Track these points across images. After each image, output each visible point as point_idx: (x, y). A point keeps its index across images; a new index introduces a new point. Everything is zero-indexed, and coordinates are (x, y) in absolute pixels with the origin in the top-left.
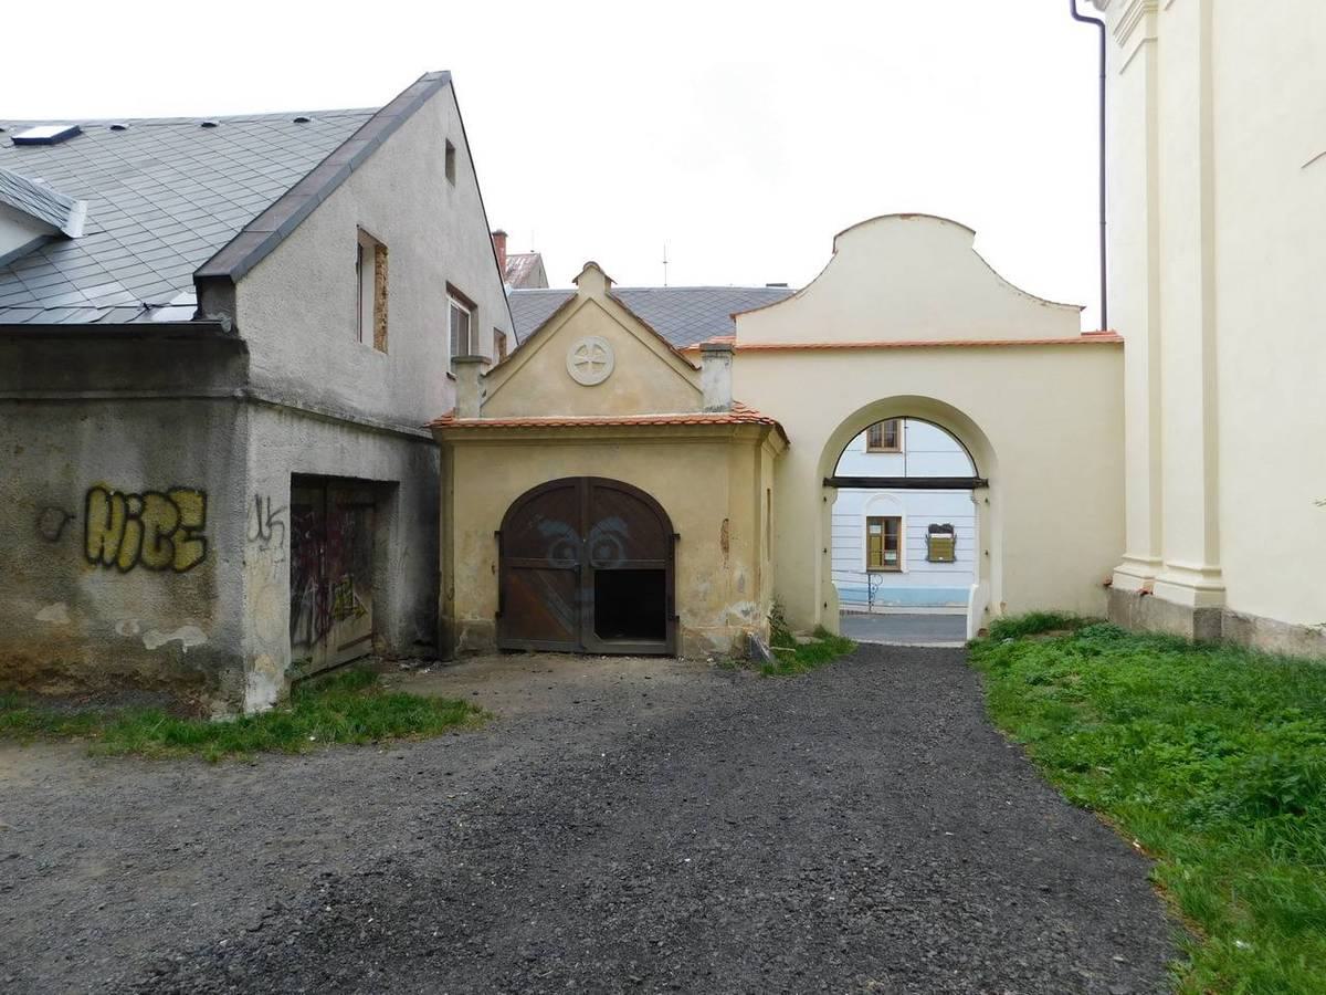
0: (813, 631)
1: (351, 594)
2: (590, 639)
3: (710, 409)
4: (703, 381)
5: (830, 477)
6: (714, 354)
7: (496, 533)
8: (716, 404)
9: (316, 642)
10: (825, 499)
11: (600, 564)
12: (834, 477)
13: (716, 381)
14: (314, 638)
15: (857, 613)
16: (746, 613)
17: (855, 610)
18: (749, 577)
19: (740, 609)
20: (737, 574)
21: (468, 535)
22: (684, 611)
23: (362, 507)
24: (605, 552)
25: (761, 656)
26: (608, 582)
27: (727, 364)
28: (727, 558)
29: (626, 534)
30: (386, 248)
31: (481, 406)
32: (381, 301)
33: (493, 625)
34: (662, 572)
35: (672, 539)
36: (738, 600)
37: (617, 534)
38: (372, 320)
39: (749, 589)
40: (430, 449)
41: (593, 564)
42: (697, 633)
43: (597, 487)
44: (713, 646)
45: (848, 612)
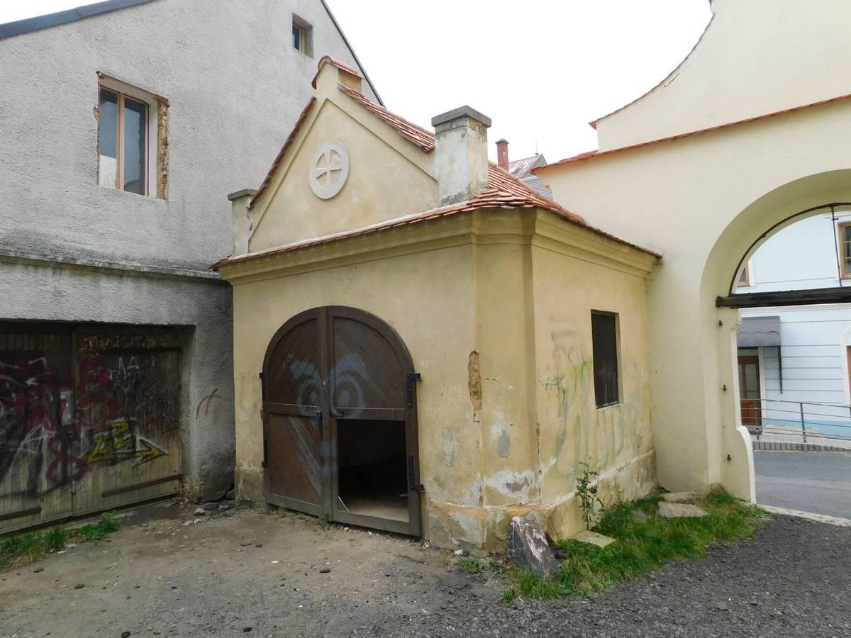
0: (705, 491)
1: (133, 438)
2: (333, 505)
3: (446, 201)
4: (437, 165)
5: (725, 294)
6: (448, 126)
7: (260, 374)
8: (453, 192)
9: (49, 492)
10: (720, 324)
11: (339, 411)
12: (731, 295)
13: (452, 161)
14: (45, 485)
15: (838, 449)
16: (515, 487)
17: (835, 446)
18: (517, 434)
19: (503, 481)
20: (496, 431)
21: (243, 378)
22: (430, 479)
23: (159, 351)
24: (345, 397)
25: (524, 557)
26: (351, 433)
27: (463, 136)
28: (479, 407)
29: (364, 375)
30: (167, 100)
31: (249, 241)
32: (162, 151)
33: (261, 476)
34: (401, 424)
35: (414, 379)
36: (501, 467)
37: (355, 374)
38: (155, 168)
39: (518, 451)
40: (218, 286)
41: (334, 412)
42: (444, 512)
43: (335, 318)
44: (462, 533)
45: (826, 448)
